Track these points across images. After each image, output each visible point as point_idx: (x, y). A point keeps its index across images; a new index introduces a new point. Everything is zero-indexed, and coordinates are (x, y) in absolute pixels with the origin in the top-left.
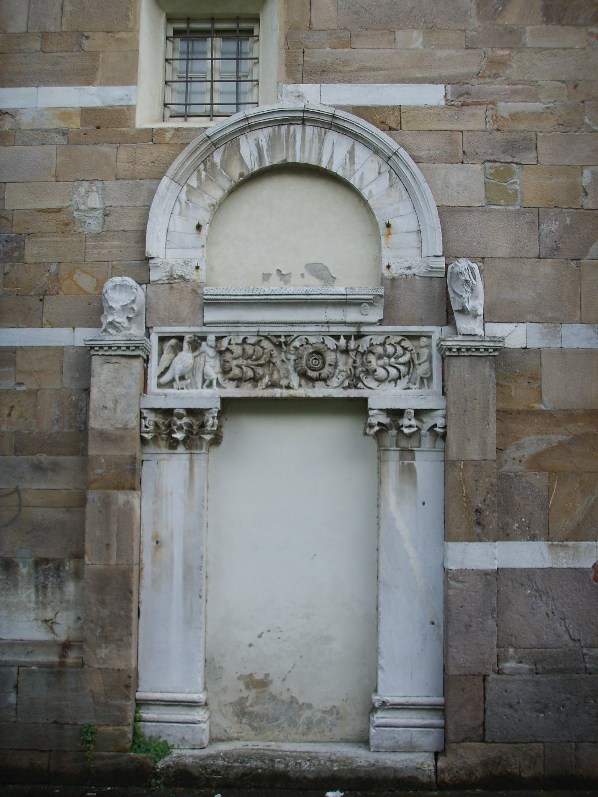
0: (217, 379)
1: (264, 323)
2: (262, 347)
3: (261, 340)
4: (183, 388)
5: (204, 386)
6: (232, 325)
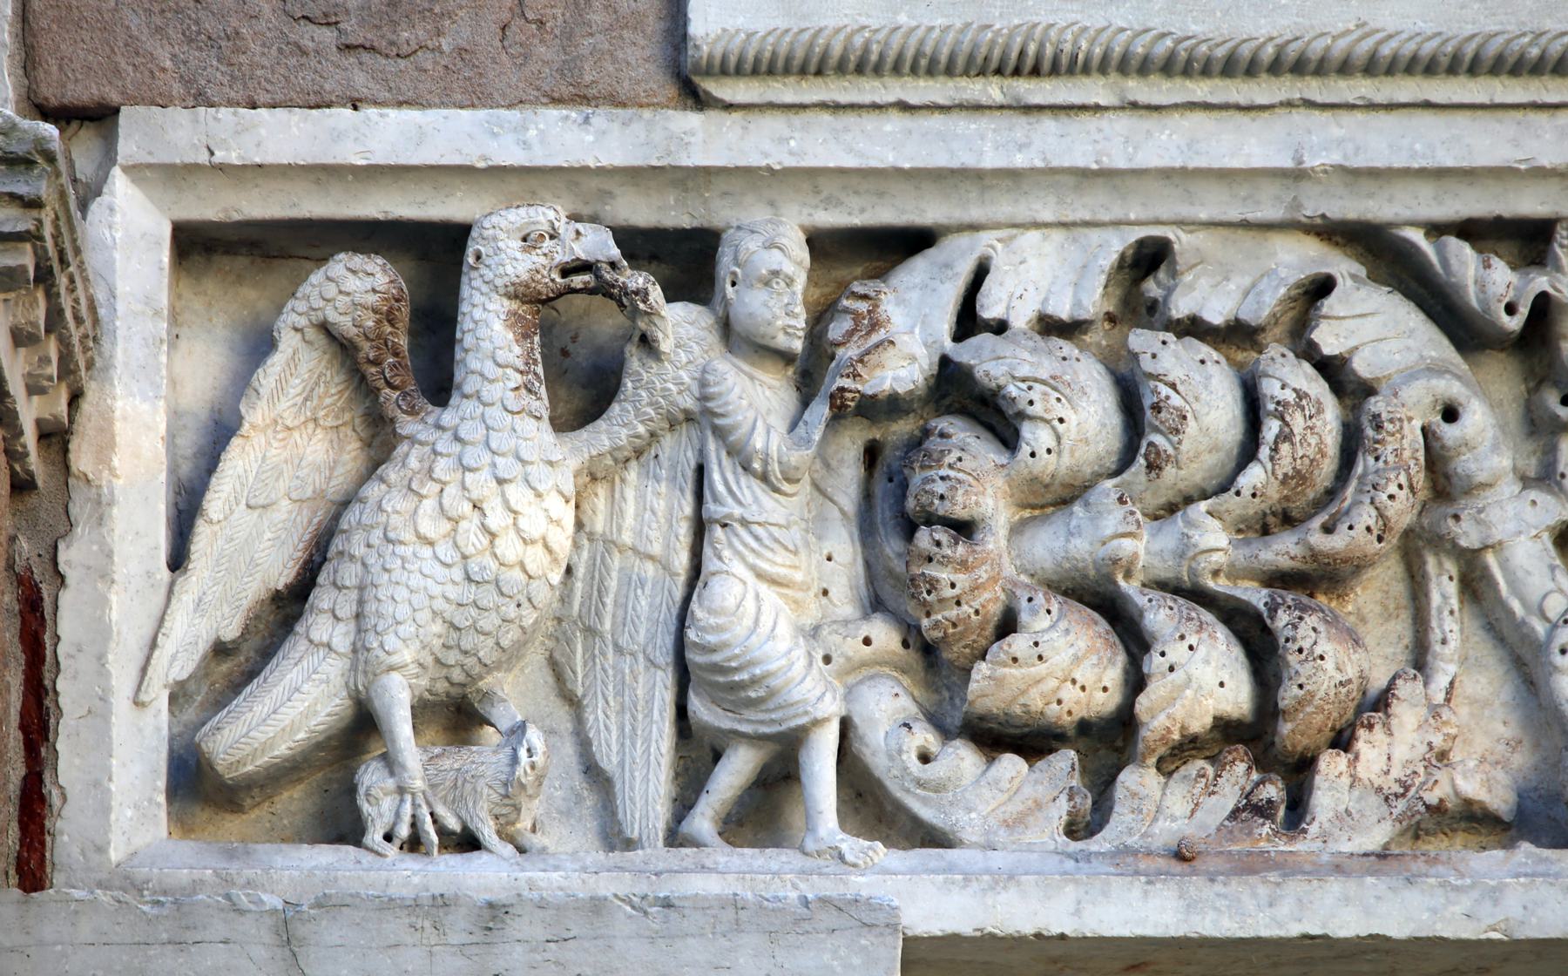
0: (846, 727)
1: (1372, 67)
2: (1332, 370)
3: (1321, 287)
4: (468, 842)
5: (703, 822)
6: (992, 90)
